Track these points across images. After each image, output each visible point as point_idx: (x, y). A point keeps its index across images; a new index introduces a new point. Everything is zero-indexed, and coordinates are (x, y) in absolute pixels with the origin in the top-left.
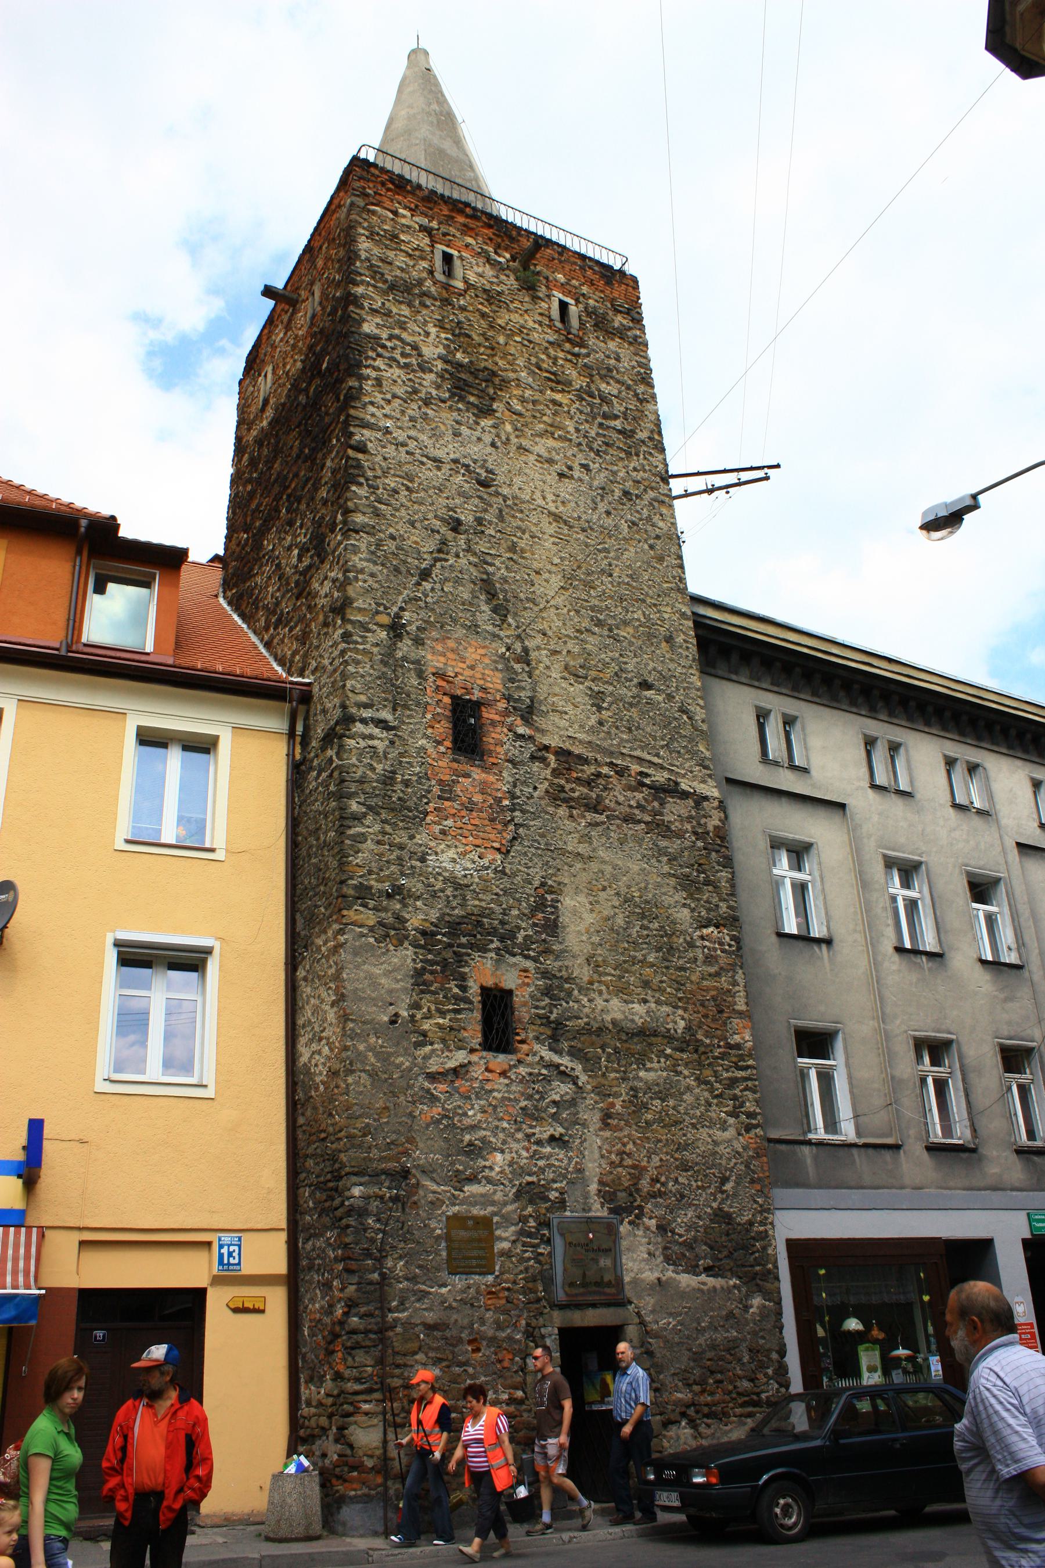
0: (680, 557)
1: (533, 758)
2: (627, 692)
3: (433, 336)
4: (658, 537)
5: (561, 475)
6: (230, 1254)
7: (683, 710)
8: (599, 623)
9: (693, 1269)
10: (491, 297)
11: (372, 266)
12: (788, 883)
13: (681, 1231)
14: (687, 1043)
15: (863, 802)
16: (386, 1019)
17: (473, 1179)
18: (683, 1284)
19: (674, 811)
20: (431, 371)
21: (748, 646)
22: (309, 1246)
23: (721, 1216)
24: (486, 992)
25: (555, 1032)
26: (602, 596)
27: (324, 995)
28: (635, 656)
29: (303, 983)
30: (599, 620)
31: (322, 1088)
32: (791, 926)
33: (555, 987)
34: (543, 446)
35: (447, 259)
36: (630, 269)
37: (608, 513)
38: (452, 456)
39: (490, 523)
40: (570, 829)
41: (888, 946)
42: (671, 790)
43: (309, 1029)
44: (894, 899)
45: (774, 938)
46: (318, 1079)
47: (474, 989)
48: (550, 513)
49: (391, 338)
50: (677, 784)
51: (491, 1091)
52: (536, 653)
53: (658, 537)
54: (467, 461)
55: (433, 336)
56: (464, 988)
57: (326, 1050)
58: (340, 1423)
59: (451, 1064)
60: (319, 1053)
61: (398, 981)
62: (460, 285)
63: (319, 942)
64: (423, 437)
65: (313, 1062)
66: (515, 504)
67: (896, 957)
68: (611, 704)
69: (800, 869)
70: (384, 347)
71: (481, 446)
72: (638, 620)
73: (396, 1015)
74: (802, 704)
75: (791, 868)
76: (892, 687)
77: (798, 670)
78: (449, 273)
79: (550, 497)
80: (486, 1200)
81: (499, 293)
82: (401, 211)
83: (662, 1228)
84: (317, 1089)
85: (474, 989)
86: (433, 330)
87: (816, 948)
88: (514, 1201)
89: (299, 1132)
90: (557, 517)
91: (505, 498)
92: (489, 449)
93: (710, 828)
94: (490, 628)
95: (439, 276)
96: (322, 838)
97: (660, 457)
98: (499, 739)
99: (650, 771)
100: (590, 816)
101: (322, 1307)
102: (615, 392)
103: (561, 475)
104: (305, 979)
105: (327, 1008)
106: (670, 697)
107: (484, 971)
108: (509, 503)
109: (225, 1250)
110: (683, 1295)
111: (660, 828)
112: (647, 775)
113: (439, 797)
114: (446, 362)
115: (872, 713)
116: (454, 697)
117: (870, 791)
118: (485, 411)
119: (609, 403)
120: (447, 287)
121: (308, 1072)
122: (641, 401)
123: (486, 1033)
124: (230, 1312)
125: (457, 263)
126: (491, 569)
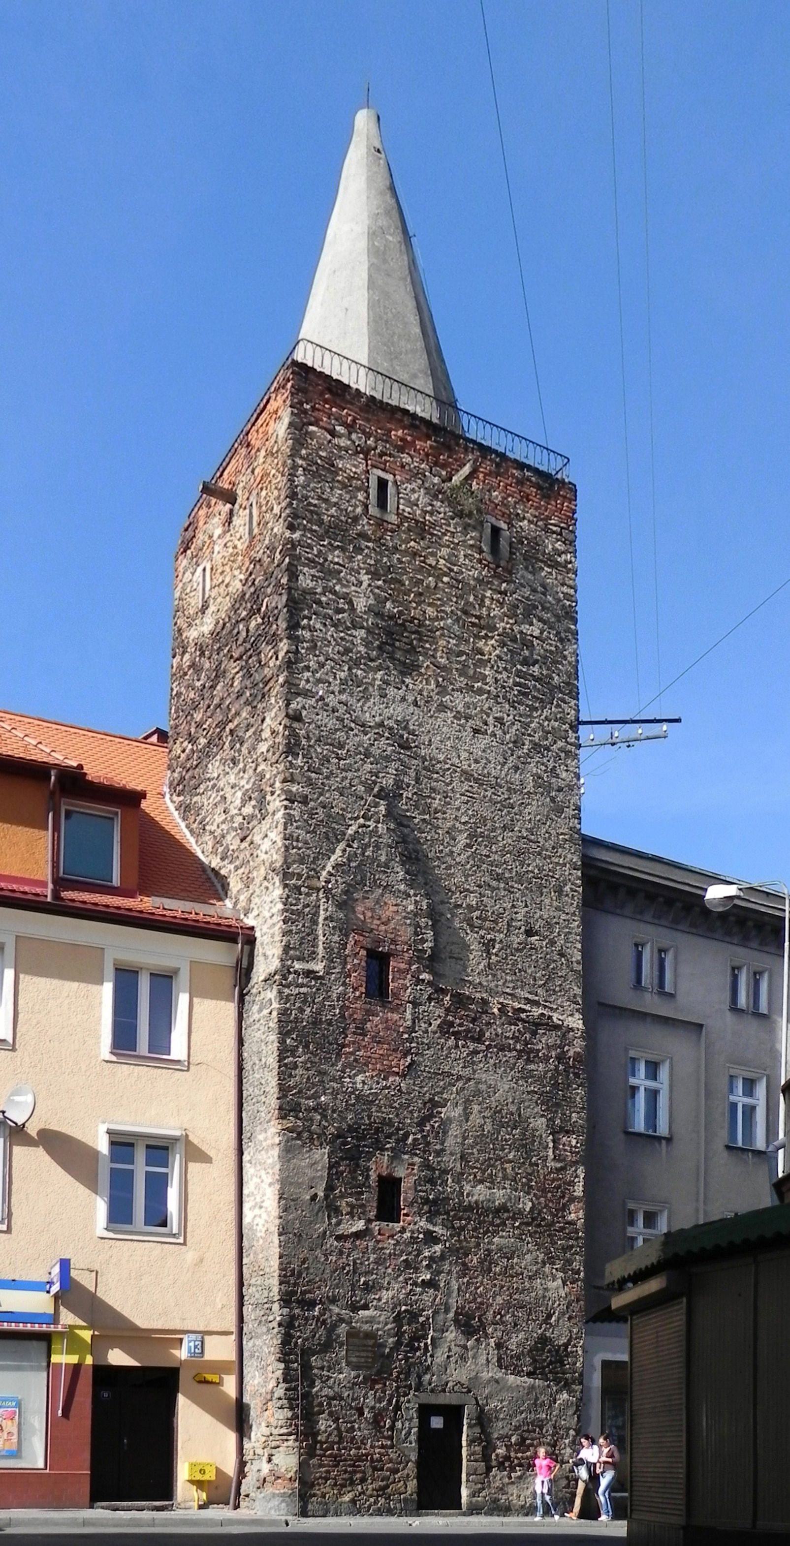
0: (578, 808)
1: (430, 999)
2: (517, 939)
3: (365, 584)
4: (560, 790)
5: (476, 731)
6: (196, 1347)
7: (562, 955)
8: (499, 878)
9: (517, 1373)
10: (421, 529)
11: (310, 504)
12: (642, 1089)
13: (514, 1347)
14: (534, 1218)
15: (722, 1024)
16: (308, 1197)
17: (366, 1307)
18: (510, 1383)
19: (544, 1041)
20: (362, 627)
21: (635, 885)
22: (251, 1344)
23: (543, 1340)
24: (381, 1179)
25: (434, 1208)
26: (503, 852)
27: (264, 1176)
28: (526, 906)
29: (248, 1165)
30: (498, 875)
31: (261, 1241)
32: (640, 1125)
33: (432, 1176)
34: (459, 701)
35: (382, 484)
36: (569, 475)
37: (517, 768)
38: (377, 719)
39: (408, 785)
40: (455, 1058)
41: (722, 1137)
42: (544, 1024)
43: (252, 1198)
44: (734, 1106)
45: (622, 1136)
46: (259, 1235)
47: (373, 1176)
48: (464, 772)
49: (325, 590)
50: (550, 1017)
51: (383, 1248)
52: (441, 907)
53: (560, 790)
54: (391, 723)
55: (365, 584)
56: (368, 1177)
57: (264, 1216)
58: (270, 1452)
59: (354, 1229)
60: (260, 1216)
61: (317, 1171)
62: (393, 519)
63: (261, 1137)
64: (352, 701)
65: (255, 1223)
66: (429, 767)
67: (725, 1154)
68: (500, 950)
69: (655, 1078)
70: (319, 603)
71: (405, 705)
72: (532, 872)
73: (316, 1195)
74: (679, 934)
75: (647, 1077)
76: (766, 918)
77: (679, 905)
78: (382, 503)
79: (464, 755)
80: (370, 1321)
81: (434, 525)
82: (338, 428)
83: (499, 1346)
84: (258, 1241)
85: (373, 1176)
86: (365, 578)
87: (657, 1144)
88: (393, 1322)
89: (244, 1267)
90: (467, 775)
91: (424, 760)
92: (411, 709)
93: (571, 1053)
94: (402, 887)
95: (373, 510)
96: (264, 1060)
97: (573, 702)
98: (402, 982)
99: (527, 1007)
100: (472, 1046)
101: (259, 1383)
102: (536, 633)
103: (476, 731)
104: (250, 1162)
105: (266, 1186)
106: (552, 943)
107: (379, 1165)
108: (426, 763)
109: (192, 1344)
110: (510, 1388)
111: (529, 1054)
112: (524, 1011)
113: (354, 1033)
114: (377, 614)
115: (745, 942)
116: (367, 950)
117: (728, 1014)
118: (408, 669)
119: (530, 646)
120: (380, 523)
121: (251, 1229)
122: (561, 640)
123: (379, 1208)
124: (195, 1383)
125: (391, 489)
126: (406, 831)
